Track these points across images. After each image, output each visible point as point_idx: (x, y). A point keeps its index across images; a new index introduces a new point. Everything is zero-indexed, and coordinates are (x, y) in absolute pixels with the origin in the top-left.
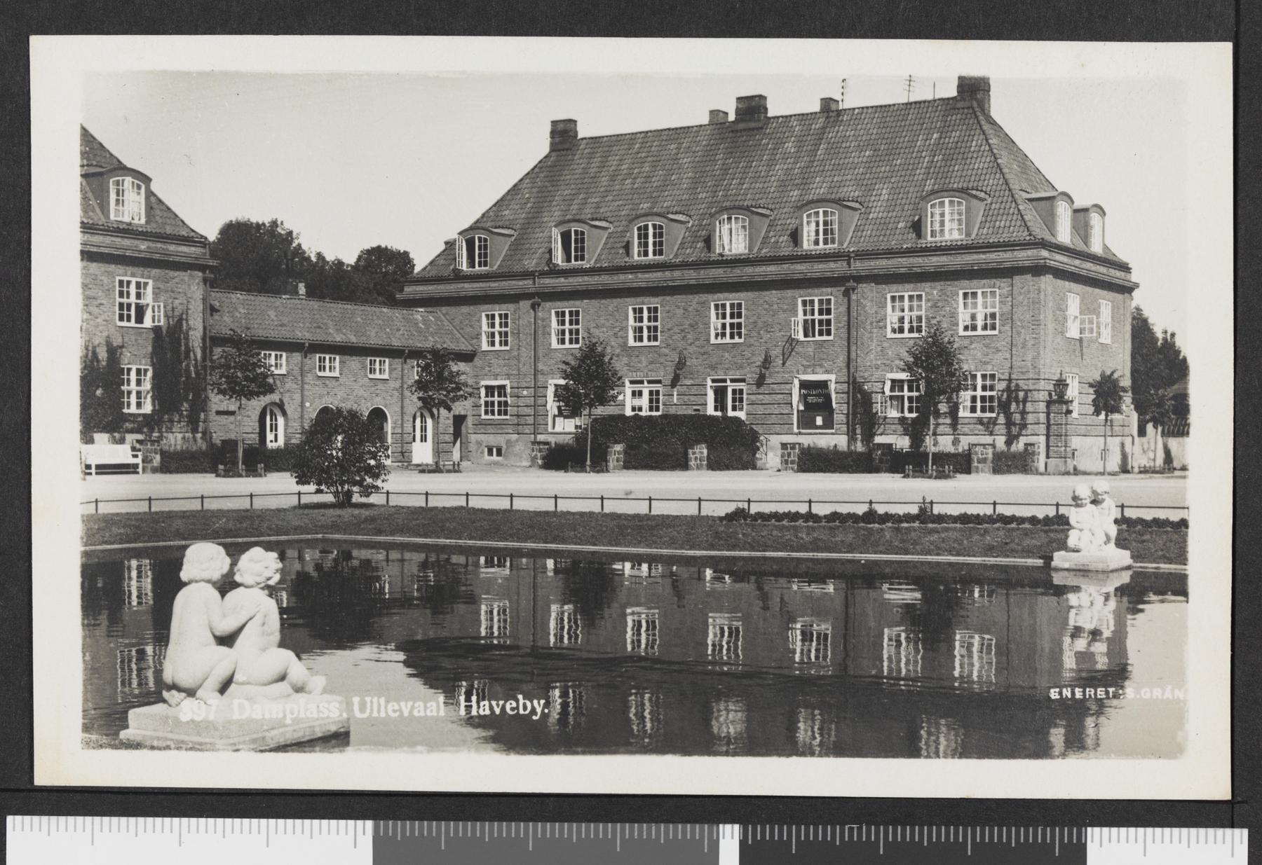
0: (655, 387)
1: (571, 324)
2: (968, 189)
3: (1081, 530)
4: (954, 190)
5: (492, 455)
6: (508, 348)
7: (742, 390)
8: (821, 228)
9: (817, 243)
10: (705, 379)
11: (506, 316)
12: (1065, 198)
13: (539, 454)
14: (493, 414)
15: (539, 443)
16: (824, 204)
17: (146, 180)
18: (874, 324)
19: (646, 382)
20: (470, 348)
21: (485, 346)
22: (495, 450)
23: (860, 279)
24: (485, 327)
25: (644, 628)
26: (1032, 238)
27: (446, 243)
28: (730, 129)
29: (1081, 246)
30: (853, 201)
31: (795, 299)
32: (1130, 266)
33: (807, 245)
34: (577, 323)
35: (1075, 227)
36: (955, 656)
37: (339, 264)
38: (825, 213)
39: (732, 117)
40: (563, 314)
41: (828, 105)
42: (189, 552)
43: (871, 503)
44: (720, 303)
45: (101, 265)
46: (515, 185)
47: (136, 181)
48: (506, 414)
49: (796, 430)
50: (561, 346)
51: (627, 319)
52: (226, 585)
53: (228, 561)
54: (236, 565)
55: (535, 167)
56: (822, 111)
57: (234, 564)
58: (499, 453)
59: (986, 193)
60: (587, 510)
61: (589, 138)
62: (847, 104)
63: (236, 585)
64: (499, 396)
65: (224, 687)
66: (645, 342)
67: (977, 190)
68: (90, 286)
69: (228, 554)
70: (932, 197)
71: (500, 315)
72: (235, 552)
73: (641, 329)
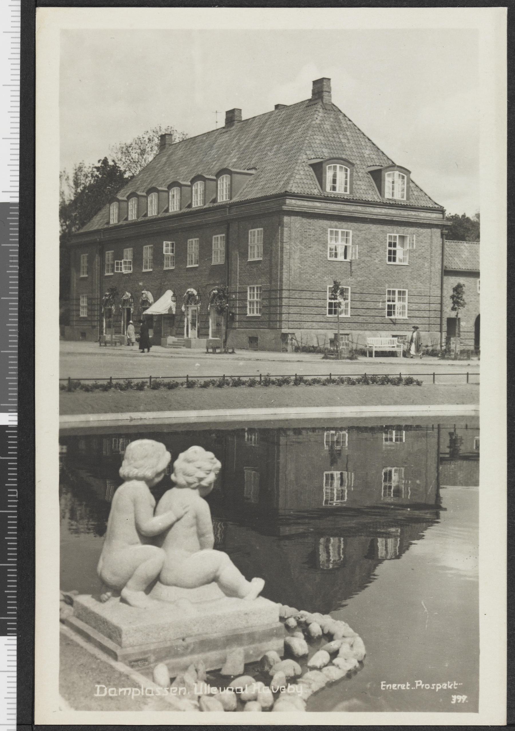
17: (408, 172)
36: (299, 610)
43: (330, 375)
45: (378, 226)
47: (401, 174)
53: (167, 456)
63: (172, 485)
68: (371, 240)
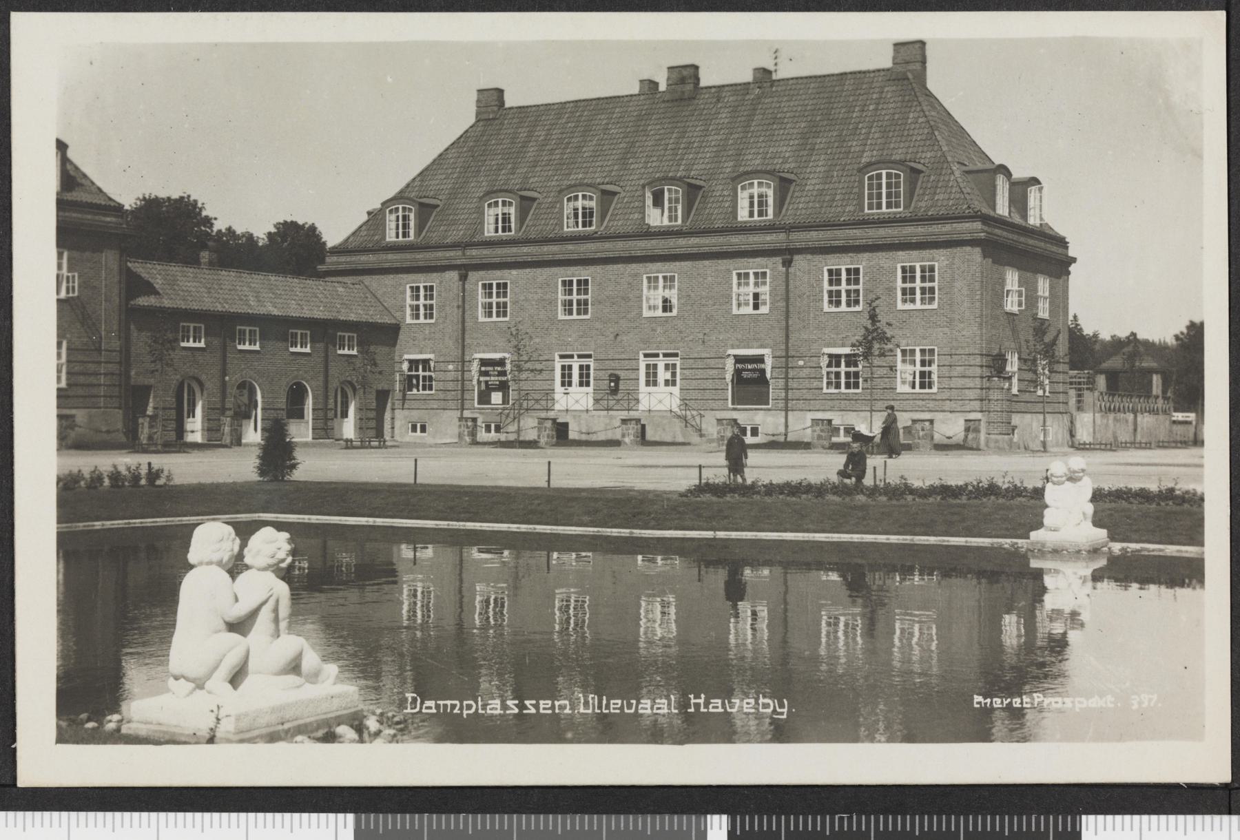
0: (585, 362)
1: (498, 296)
2: (905, 161)
3: (1057, 508)
4: (892, 162)
5: (416, 431)
6: (432, 321)
7: (675, 364)
8: (401, 223)
9: (497, 231)
10: (638, 353)
11: (432, 288)
12: (1002, 170)
13: (466, 430)
14: (838, 386)
15: (466, 419)
16: (760, 175)
18: (812, 298)
19: (576, 357)
20: (393, 321)
21: (409, 320)
22: (419, 425)
23: (799, 251)
24: (409, 301)
25: (491, 606)
26: (970, 210)
27: (369, 213)
28: (661, 100)
29: (1017, 219)
30: (788, 172)
31: (729, 272)
32: (1067, 240)
33: (391, 237)
34: (431, 298)
35: (1012, 201)
37: (250, 237)
38: (404, 209)
39: (663, 87)
40: (418, 288)
41: (763, 75)
42: (198, 532)
44: (652, 275)
46: (441, 155)
48: (431, 389)
49: (730, 405)
50: (834, 309)
51: (895, 280)
52: (236, 567)
54: (246, 546)
55: (461, 136)
56: (756, 81)
57: (244, 545)
58: (498, 429)
59: (924, 164)
60: (652, 489)
61: (516, 108)
62: (779, 75)
64: (424, 370)
65: (235, 679)
66: (422, 320)
67: (915, 162)
69: (237, 534)
70: (869, 169)
71: (425, 287)
72: (245, 532)
73: (417, 308)
